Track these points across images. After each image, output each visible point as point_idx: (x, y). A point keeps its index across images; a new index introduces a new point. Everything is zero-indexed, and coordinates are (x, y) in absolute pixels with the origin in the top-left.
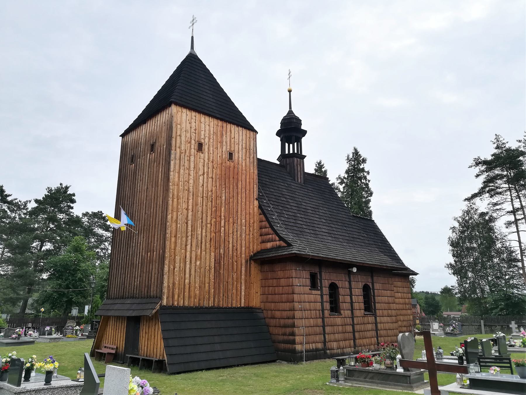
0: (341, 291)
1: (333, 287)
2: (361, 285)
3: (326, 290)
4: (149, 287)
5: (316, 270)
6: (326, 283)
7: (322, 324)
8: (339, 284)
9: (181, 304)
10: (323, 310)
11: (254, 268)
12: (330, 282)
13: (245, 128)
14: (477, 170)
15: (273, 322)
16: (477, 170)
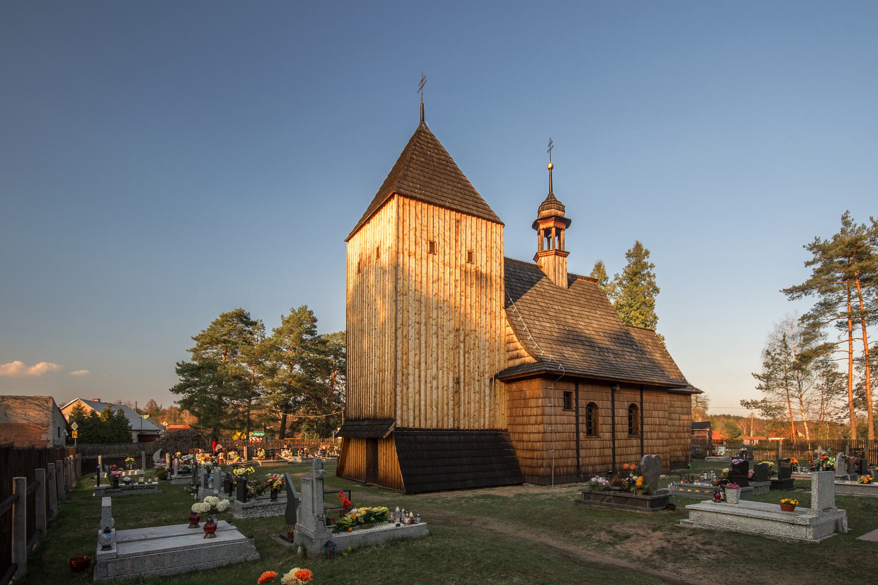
0: (601, 412)
1: (591, 407)
2: (626, 405)
3: (582, 411)
4: (382, 408)
5: (572, 388)
6: (583, 403)
7: (575, 447)
8: (599, 404)
9: (417, 426)
10: (578, 432)
11: (501, 387)
12: (588, 402)
13: (493, 221)
14: (811, 256)
15: (520, 445)
16: (811, 256)
